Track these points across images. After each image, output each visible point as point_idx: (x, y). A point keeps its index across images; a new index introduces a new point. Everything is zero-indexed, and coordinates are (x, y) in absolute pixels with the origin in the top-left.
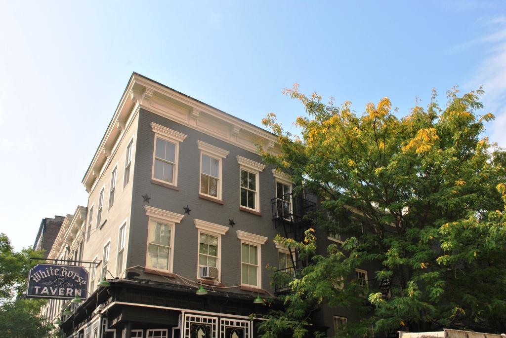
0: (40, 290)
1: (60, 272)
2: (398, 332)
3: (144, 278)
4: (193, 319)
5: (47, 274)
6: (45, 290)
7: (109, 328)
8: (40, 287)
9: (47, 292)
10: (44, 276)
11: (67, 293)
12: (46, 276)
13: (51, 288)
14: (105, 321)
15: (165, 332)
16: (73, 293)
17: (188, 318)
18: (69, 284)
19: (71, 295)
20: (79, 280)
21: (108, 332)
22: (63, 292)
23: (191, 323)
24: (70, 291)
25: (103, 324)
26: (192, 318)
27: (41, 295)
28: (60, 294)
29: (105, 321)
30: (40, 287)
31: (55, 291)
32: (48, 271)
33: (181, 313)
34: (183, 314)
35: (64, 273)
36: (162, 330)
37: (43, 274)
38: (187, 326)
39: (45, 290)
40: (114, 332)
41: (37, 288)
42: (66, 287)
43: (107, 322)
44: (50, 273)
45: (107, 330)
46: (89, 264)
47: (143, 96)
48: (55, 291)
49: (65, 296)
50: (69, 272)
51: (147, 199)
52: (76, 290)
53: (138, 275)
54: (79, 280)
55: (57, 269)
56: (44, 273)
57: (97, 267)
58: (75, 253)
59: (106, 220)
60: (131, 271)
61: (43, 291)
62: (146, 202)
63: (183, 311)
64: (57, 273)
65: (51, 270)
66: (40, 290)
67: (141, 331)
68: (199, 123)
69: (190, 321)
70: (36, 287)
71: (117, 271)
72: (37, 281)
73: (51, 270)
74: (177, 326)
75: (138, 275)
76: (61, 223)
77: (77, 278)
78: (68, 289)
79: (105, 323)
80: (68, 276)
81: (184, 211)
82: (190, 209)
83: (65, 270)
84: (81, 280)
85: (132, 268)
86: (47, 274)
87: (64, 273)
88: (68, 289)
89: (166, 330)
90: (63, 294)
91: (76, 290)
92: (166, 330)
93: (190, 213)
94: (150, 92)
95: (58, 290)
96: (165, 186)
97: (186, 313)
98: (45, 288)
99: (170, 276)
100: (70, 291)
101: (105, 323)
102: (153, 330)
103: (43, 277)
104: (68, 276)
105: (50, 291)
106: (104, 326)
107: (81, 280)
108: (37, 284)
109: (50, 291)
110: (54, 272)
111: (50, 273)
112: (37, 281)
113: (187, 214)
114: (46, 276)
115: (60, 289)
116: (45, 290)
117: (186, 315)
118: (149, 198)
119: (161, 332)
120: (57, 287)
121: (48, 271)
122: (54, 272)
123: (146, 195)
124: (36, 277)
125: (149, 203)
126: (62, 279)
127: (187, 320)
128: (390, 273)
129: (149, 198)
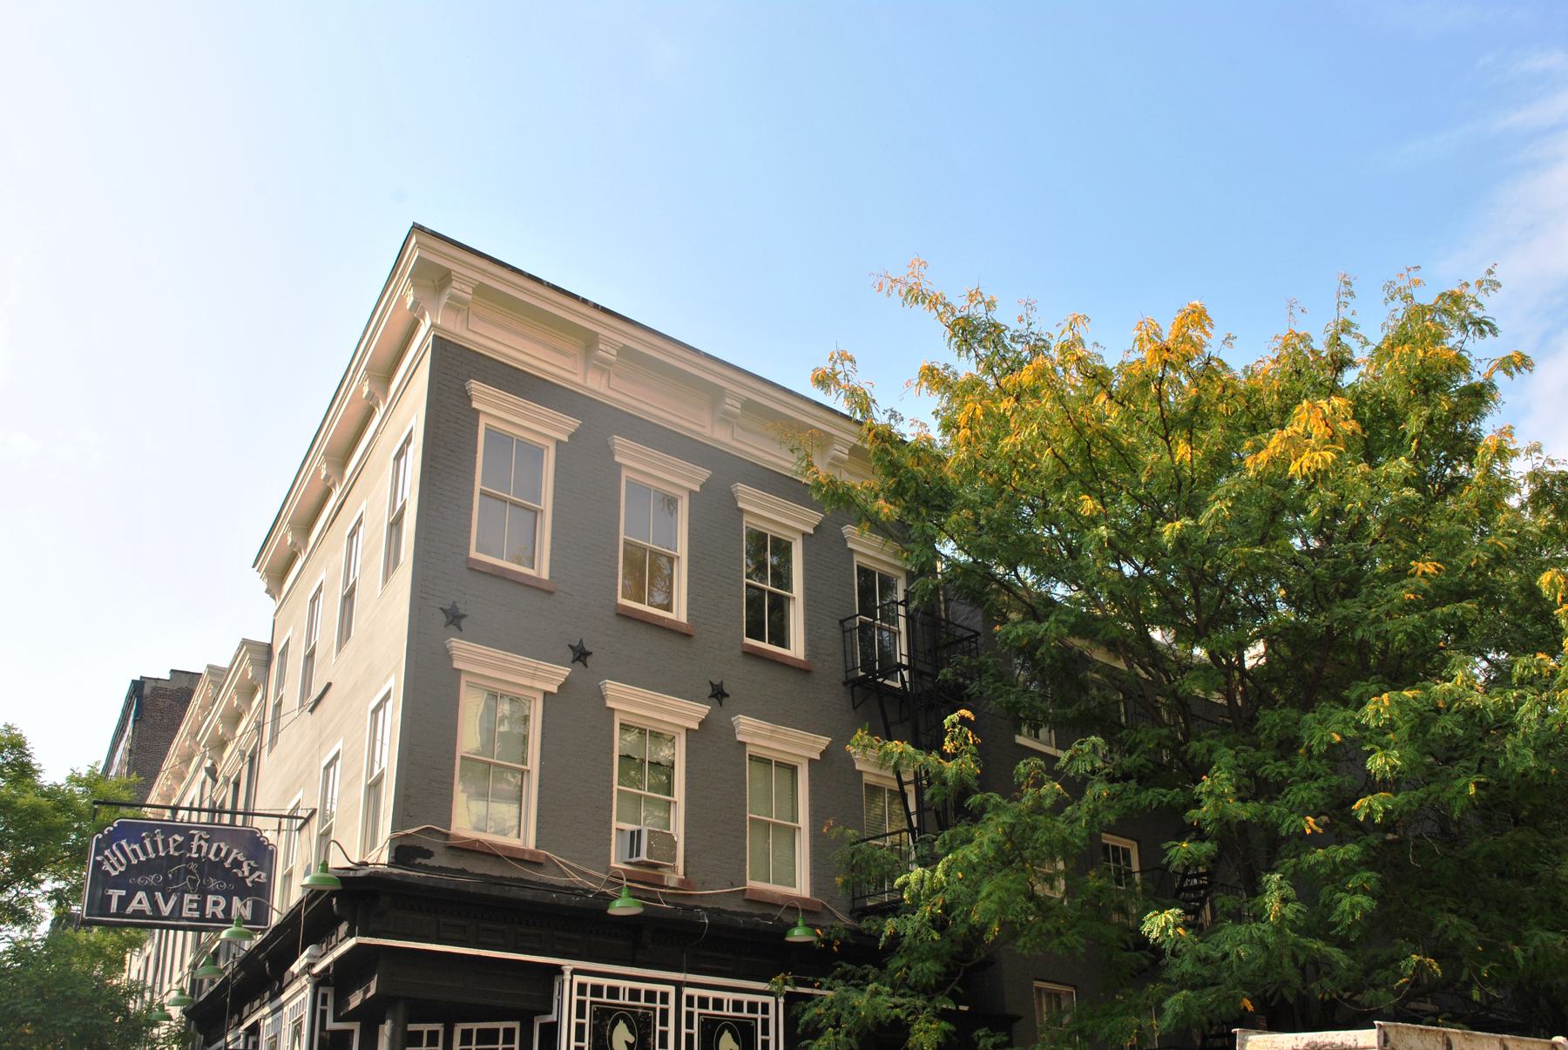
0: (124, 902)
1: (184, 846)
4: (597, 990)
5: (145, 852)
7: (336, 1020)
8: (123, 893)
9: (146, 906)
10: (137, 857)
11: (209, 910)
12: (143, 858)
14: (325, 997)
16: (227, 911)
17: (582, 988)
19: (220, 915)
20: (246, 869)
21: (333, 1032)
22: (195, 906)
23: (592, 1003)
24: (216, 903)
25: (319, 1007)
29: (325, 997)
30: (123, 893)
31: (171, 903)
32: (147, 842)
33: (562, 973)
34: (567, 976)
35: (200, 847)
36: (501, 1026)
37: (134, 851)
38: (581, 1014)
39: (140, 901)
41: (116, 894)
44: (156, 850)
45: (331, 1025)
47: (445, 300)
48: (171, 903)
49: (202, 918)
50: (215, 846)
51: (454, 619)
53: (428, 854)
54: (246, 869)
55: (177, 837)
56: (136, 847)
57: (300, 829)
58: (231, 786)
59: (329, 685)
60: (407, 842)
61: (134, 905)
63: (568, 965)
64: (176, 849)
65: (159, 839)
66: (124, 902)
67: (438, 1027)
70: (111, 892)
73: (159, 839)
75: (428, 854)
77: (237, 864)
78: (211, 898)
79: (324, 1002)
80: (211, 856)
81: (570, 655)
83: (201, 838)
84: (252, 871)
86: (145, 852)
87: (200, 847)
88: (211, 898)
89: (516, 1025)
90: (196, 914)
91: (236, 899)
92: (516, 1025)
97: (575, 972)
98: (141, 895)
99: (527, 857)
100: (216, 903)
101: (324, 1002)
102: (475, 1026)
103: (135, 862)
105: (154, 904)
106: (323, 1013)
107: (252, 871)
108: (116, 883)
109: (154, 904)
110: (166, 845)
111: (156, 850)
112: (114, 873)
113: (579, 664)
114: (143, 858)
115: (187, 897)
116: (140, 902)
117: (578, 979)
121: (147, 842)
122: (166, 845)
124: (113, 860)
126: (193, 866)
128: (1207, 847)
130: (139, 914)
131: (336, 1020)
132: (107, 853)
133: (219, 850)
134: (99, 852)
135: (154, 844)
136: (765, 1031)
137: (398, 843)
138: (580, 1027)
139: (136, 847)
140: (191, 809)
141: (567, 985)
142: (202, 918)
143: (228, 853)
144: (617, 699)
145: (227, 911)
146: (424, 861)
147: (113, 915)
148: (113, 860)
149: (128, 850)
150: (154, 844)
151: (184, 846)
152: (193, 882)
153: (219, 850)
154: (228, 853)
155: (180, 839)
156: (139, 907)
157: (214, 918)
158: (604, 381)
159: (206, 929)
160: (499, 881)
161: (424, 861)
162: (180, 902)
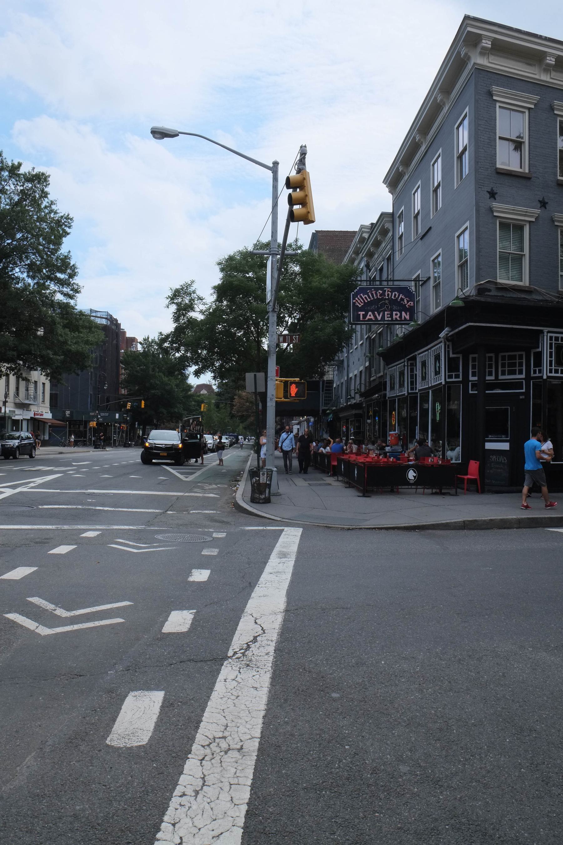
0: (365, 316)
1: (383, 294)
2: (359, 313)
3: (496, 294)
4: (557, 339)
5: (369, 298)
6: (370, 316)
7: (453, 354)
8: (364, 313)
9: (372, 317)
10: (367, 299)
11: (394, 317)
12: (369, 300)
13: (376, 313)
14: (448, 346)
15: (522, 355)
16: (401, 317)
17: (551, 338)
18: (395, 307)
19: (399, 319)
20: (405, 301)
21: (452, 358)
22: (389, 316)
23: (555, 344)
24: (396, 315)
25: (447, 349)
26: (555, 337)
27: (366, 321)
28: (386, 319)
29: (448, 346)
30: (364, 313)
31: (381, 315)
32: (370, 294)
33: (543, 333)
34: (545, 334)
35: (388, 295)
36: (517, 353)
37: (365, 298)
38: (551, 348)
39: (370, 316)
40: (459, 358)
41: (362, 313)
42: (392, 311)
43: (451, 347)
44: (373, 296)
45: (451, 355)
46: (395, 279)
47: (479, 50)
48: (381, 315)
49: (392, 320)
50: (394, 293)
51: (493, 195)
52: (403, 313)
53: (490, 291)
54: (405, 301)
55: (380, 291)
56: (366, 296)
57: (422, 285)
58: (378, 272)
59: (430, 228)
60: (481, 287)
61: (368, 317)
62: (492, 199)
63: (546, 330)
64: (380, 296)
65: (374, 292)
66: (365, 316)
67: (492, 355)
68: (553, 74)
69: (554, 342)
70: (359, 313)
71: (457, 288)
72: (360, 306)
73: (374, 292)
74: (538, 348)
75: (490, 291)
76: (354, 236)
77: (402, 299)
78: (394, 313)
79: (448, 348)
80: (393, 297)
81: (539, 205)
82: (546, 201)
83: (388, 291)
84: (408, 302)
85: (482, 282)
86: (369, 298)
87: (388, 295)
88: (394, 313)
89: (524, 353)
90: (390, 319)
91: (403, 313)
92: (524, 353)
93: (547, 206)
94: (487, 41)
95: (384, 314)
96: (513, 173)
97: (548, 332)
98: (370, 313)
99: (527, 289)
100: (396, 315)
101: (448, 348)
102: (507, 354)
103: (366, 301)
104: (393, 297)
105: (375, 317)
106: (449, 351)
107: (408, 302)
108: (361, 309)
109: (375, 317)
110: (377, 295)
111: (373, 296)
112: (360, 306)
113: (543, 208)
114: (369, 300)
115: (386, 313)
116: (370, 316)
117: (549, 335)
118: (496, 193)
119: (516, 355)
120: (382, 311)
121: (370, 294)
122: (377, 295)
123: (492, 189)
124: (359, 301)
125: (495, 199)
126: (387, 301)
127: (550, 340)
128: (42, 206)
129: (496, 193)
130: (370, 320)
131: (453, 354)
132: (356, 299)
133: (395, 295)
134: (354, 299)
135: (372, 295)
136: (551, 362)
137: (478, 287)
138: (551, 353)
139: (366, 296)
140: (387, 281)
141: (545, 337)
142: (392, 320)
143: (399, 296)
144: (559, 221)
145: (401, 317)
146: (488, 293)
147: (362, 321)
148: (359, 301)
149: (364, 297)
150: (372, 295)
151: (383, 294)
152: (388, 307)
153: (395, 295)
154: (399, 296)
155: (381, 292)
156: (370, 317)
157: (396, 320)
158: (549, 76)
159: (404, 324)
160: (519, 299)
161: (488, 293)
162: (384, 315)
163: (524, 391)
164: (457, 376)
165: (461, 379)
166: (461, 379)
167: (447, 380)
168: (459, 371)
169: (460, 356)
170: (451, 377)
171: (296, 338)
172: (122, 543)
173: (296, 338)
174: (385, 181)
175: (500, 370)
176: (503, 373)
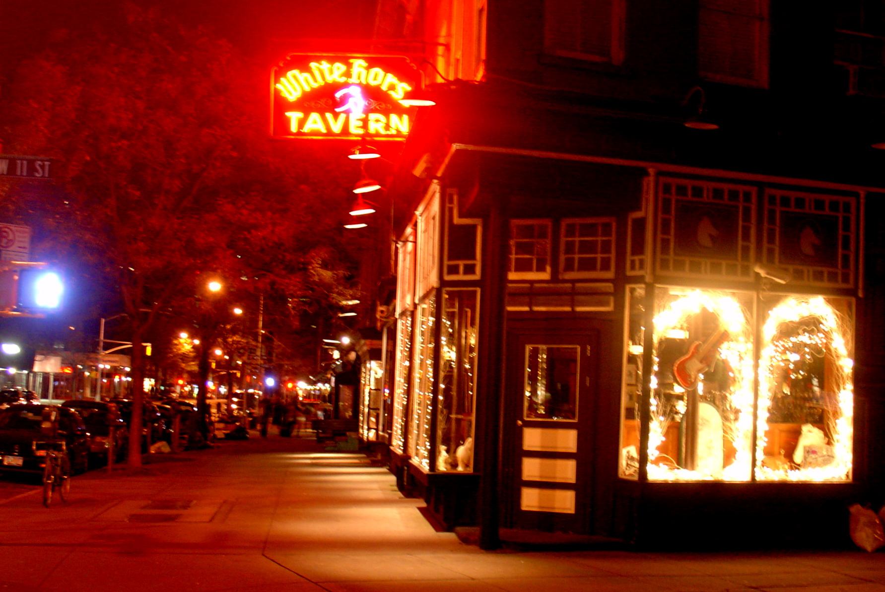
7: (461, 216)
26: (457, 273)
40: (474, 227)
45: (457, 220)
79: (451, 202)
102: (578, 221)
106: (451, 210)
163: (576, 421)
164: (470, 270)
165: (477, 276)
166: (477, 276)
167: (447, 278)
168: (474, 258)
169: (478, 222)
170: (453, 270)
171: (42, 167)
172: (467, 286)
173: (42, 167)
174: (781, 325)
175: (562, 258)
176: (569, 267)
